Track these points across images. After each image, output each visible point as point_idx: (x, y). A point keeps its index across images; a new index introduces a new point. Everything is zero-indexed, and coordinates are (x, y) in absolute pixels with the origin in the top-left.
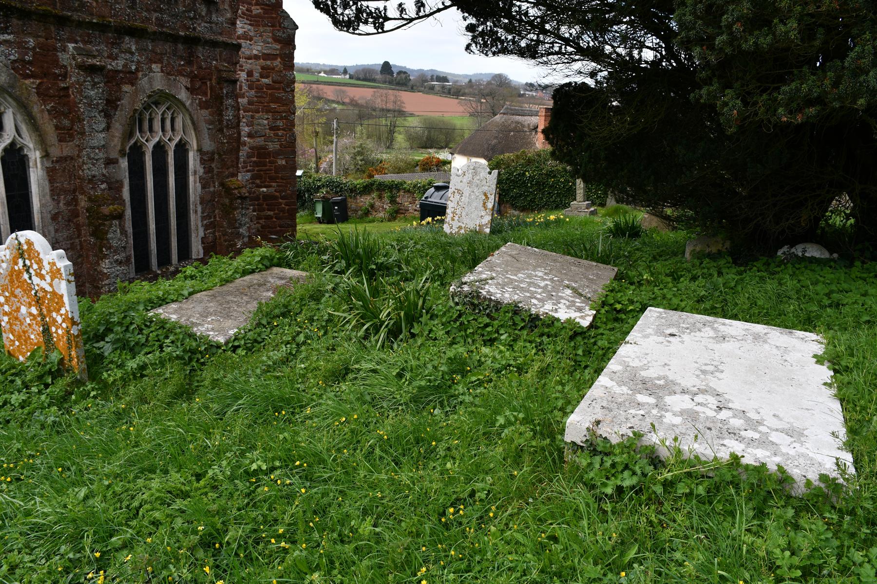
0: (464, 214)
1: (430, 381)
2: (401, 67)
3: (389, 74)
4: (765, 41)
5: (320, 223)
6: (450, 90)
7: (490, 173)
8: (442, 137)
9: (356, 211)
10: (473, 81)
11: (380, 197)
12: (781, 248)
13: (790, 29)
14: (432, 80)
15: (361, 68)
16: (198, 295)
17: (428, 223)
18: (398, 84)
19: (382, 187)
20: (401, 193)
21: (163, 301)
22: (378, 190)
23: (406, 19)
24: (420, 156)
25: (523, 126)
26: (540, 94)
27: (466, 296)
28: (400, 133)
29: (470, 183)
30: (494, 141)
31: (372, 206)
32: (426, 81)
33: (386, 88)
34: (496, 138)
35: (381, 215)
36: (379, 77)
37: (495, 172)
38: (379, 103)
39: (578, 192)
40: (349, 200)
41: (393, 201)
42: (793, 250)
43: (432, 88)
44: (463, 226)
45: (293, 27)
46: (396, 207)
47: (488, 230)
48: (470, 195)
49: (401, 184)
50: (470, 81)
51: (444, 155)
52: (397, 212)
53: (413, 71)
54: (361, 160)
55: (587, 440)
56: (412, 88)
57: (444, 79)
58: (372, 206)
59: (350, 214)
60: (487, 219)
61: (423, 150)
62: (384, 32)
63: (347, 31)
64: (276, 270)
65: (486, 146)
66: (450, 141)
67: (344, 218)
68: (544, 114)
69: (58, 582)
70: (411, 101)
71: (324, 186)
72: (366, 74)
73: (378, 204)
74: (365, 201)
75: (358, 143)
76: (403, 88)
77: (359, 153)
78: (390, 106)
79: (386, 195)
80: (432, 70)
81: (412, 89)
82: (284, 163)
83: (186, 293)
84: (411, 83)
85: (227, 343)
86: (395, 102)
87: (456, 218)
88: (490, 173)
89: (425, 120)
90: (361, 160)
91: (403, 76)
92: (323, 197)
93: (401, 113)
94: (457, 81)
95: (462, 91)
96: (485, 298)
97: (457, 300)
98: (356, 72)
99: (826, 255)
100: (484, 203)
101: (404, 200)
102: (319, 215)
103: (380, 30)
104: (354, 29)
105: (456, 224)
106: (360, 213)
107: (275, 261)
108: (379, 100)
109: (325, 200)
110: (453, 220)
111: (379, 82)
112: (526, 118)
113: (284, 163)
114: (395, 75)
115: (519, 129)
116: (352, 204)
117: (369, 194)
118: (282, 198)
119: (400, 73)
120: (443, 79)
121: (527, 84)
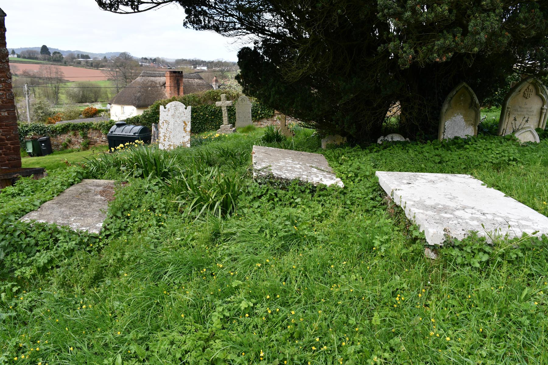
0: (171, 136)
1: (286, 232)
2: (55, 49)
3: (47, 54)
5: (31, 156)
6: (92, 64)
7: (186, 108)
8: (92, 95)
9: (57, 146)
10: (107, 57)
11: (75, 135)
12: (379, 138)
14: (78, 57)
15: (25, 50)
16: (46, 204)
17: (122, 148)
18: (55, 61)
19: (75, 128)
20: (91, 131)
21: (24, 212)
22: (73, 130)
23: (155, 3)
24: (83, 107)
25: (156, 83)
26: (152, 64)
27: (266, 178)
28: (62, 94)
29: (173, 115)
30: (139, 94)
31: (70, 141)
32: (75, 58)
33: (47, 64)
35: (77, 146)
36: (40, 56)
37: (189, 108)
38: (45, 74)
39: (224, 119)
40: (51, 138)
41: (85, 136)
42: (386, 138)
43: (79, 63)
44: (172, 144)
45: (2, 14)
46: (88, 140)
47: (189, 145)
48: (174, 123)
49: (90, 125)
50: (105, 58)
51: (98, 106)
52: (89, 144)
53: (64, 52)
54: (42, 113)
55: (445, 242)
56: (65, 63)
57: (87, 57)
58: (70, 141)
59: (53, 148)
60: (188, 138)
61: (80, 104)
62: (139, 11)
63: (111, 10)
64: (87, 181)
65: (133, 98)
66: (98, 97)
67: (49, 151)
68: (169, 75)
70: (67, 72)
71: (31, 130)
72: (30, 54)
73: (74, 139)
74: (64, 138)
75: (38, 101)
76: (59, 64)
77: (40, 108)
78: (53, 75)
79: (80, 133)
80: (77, 51)
81: (65, 64)
82: (6, 114)
83: (37, 203)
84: (64, 60)
85: (101, 233)
86: (57, 73)
87: (167, 139)
88: (186, 108)
89: (79, 84)
90: (42, 113)
91: (58, 55)
92: (32, 138)
93: (60, 80)
94: (96, 58)
95: (101, 64)
96: (278, 178)
97: (259, 181)
98: (23, 53)
99: (402, 139)
100: (184, 128)
101: (93, 135)
102: (30, 150)
103: (136, 10)
104: (115, 9)
105: (167, 143)
106: (61, 147)
107: (84, 174)
108: (45, 72)
109: (34, 140)
110: (165, 141)
111: (41, 60)
112: (157, 78)
113: (6, 114)
114: (52, 55)
115: (154, 85)
116: (54, 141)
117: (67, 133)
118: (7, 140)
119: (55, 53)
120: (86, 57)
121: (143, 58)
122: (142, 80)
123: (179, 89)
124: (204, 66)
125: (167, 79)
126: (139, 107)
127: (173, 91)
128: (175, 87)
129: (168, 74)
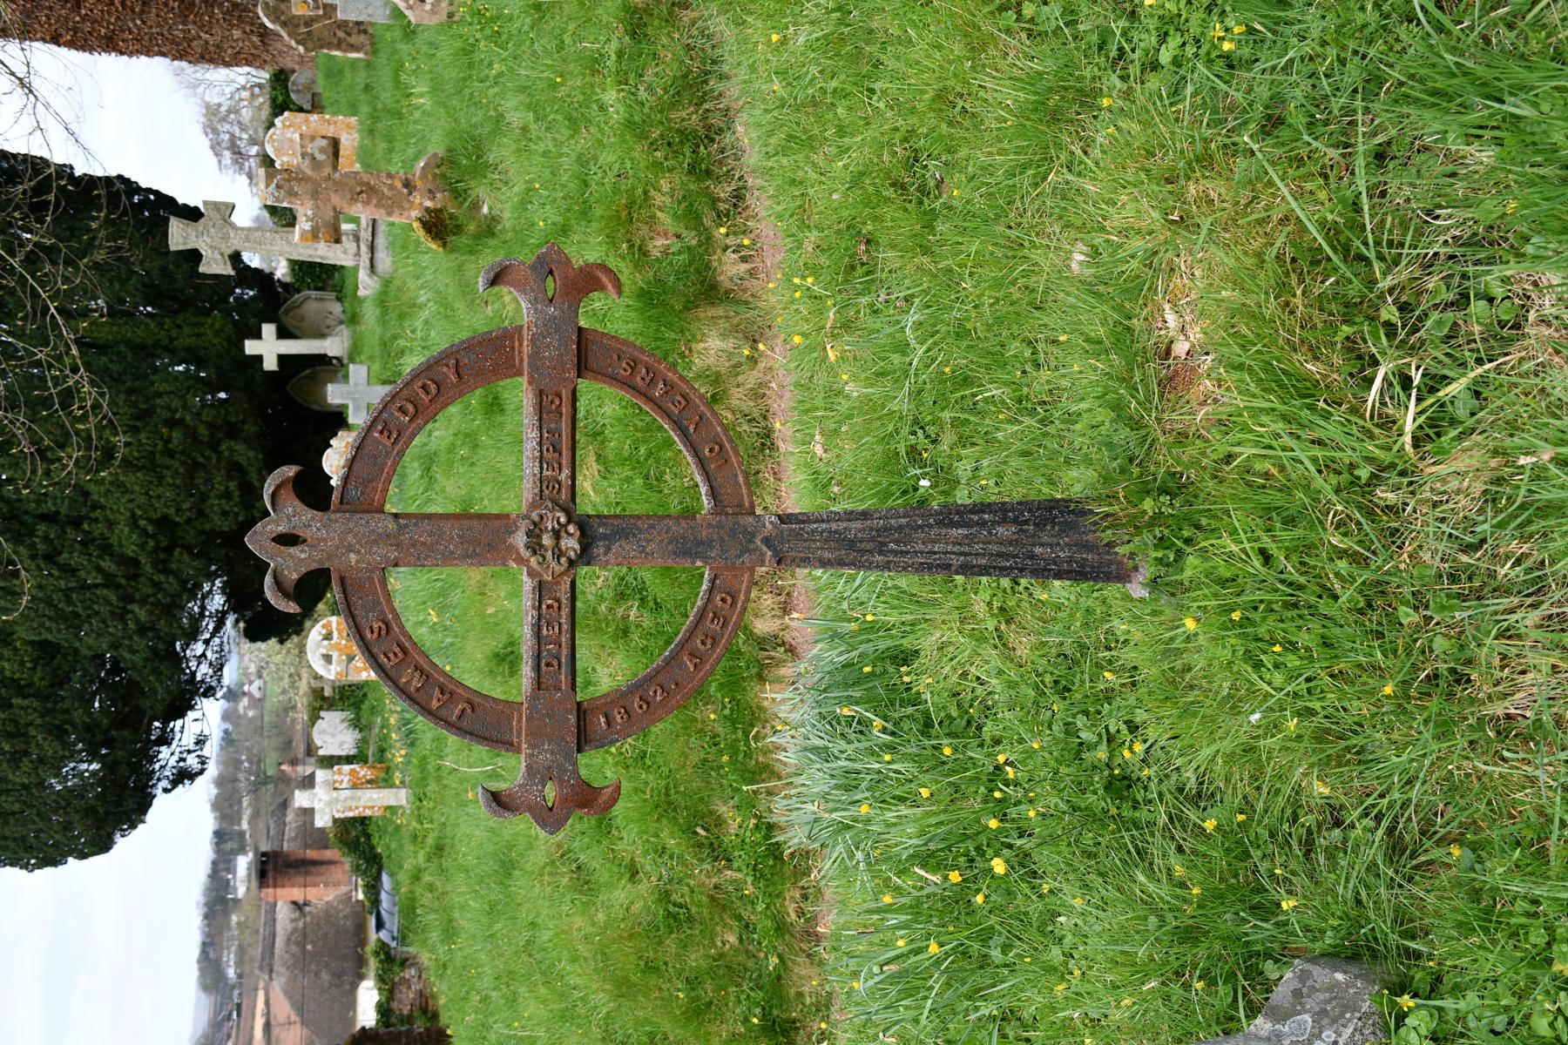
4: (237, 493)
13: (233, 485)
20: (395, 1005)
25: (295, 930)
29: (333, 736)
30: (325, 976)
34: (317, 974)
65: (334, 991)
68: (270, 890)
69: (9, 317)
115: (300, 937)
122: (283, 970)
123: (314, 863)
124: (231, 869)
125: (285, 896)
126: (361, 977)
127: (319, 879)
128: (307, 873)
129: (269, 892)
